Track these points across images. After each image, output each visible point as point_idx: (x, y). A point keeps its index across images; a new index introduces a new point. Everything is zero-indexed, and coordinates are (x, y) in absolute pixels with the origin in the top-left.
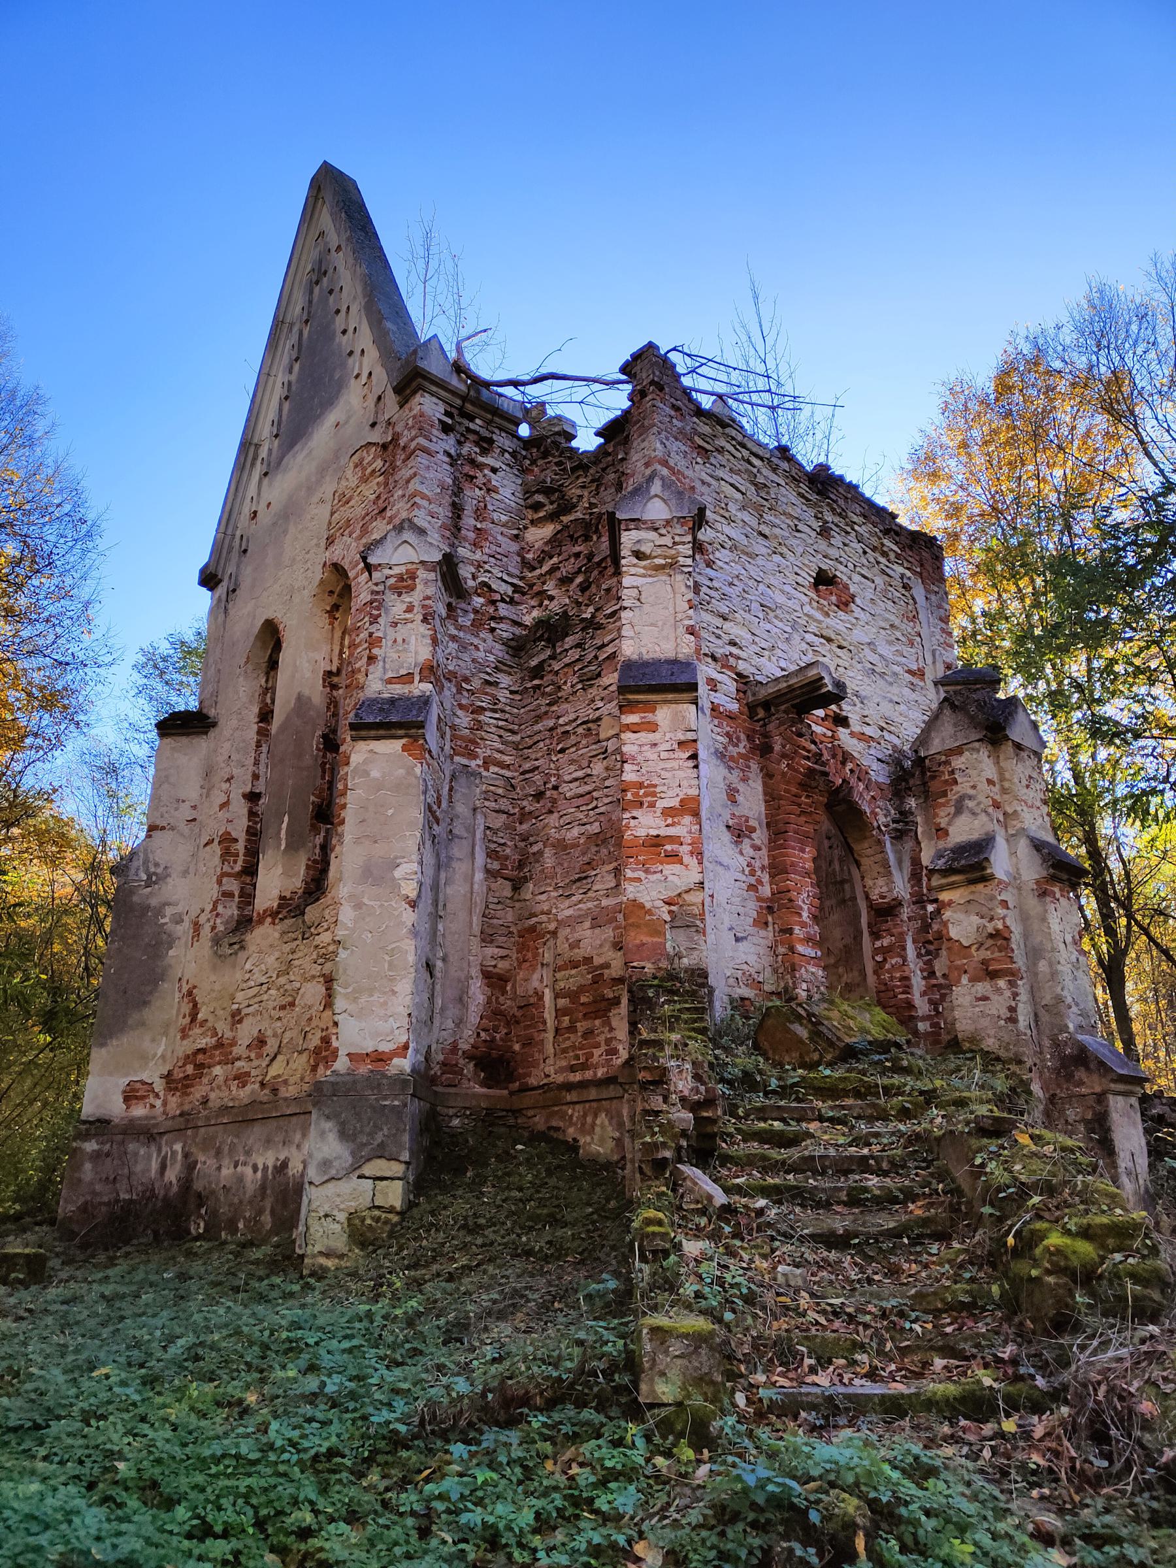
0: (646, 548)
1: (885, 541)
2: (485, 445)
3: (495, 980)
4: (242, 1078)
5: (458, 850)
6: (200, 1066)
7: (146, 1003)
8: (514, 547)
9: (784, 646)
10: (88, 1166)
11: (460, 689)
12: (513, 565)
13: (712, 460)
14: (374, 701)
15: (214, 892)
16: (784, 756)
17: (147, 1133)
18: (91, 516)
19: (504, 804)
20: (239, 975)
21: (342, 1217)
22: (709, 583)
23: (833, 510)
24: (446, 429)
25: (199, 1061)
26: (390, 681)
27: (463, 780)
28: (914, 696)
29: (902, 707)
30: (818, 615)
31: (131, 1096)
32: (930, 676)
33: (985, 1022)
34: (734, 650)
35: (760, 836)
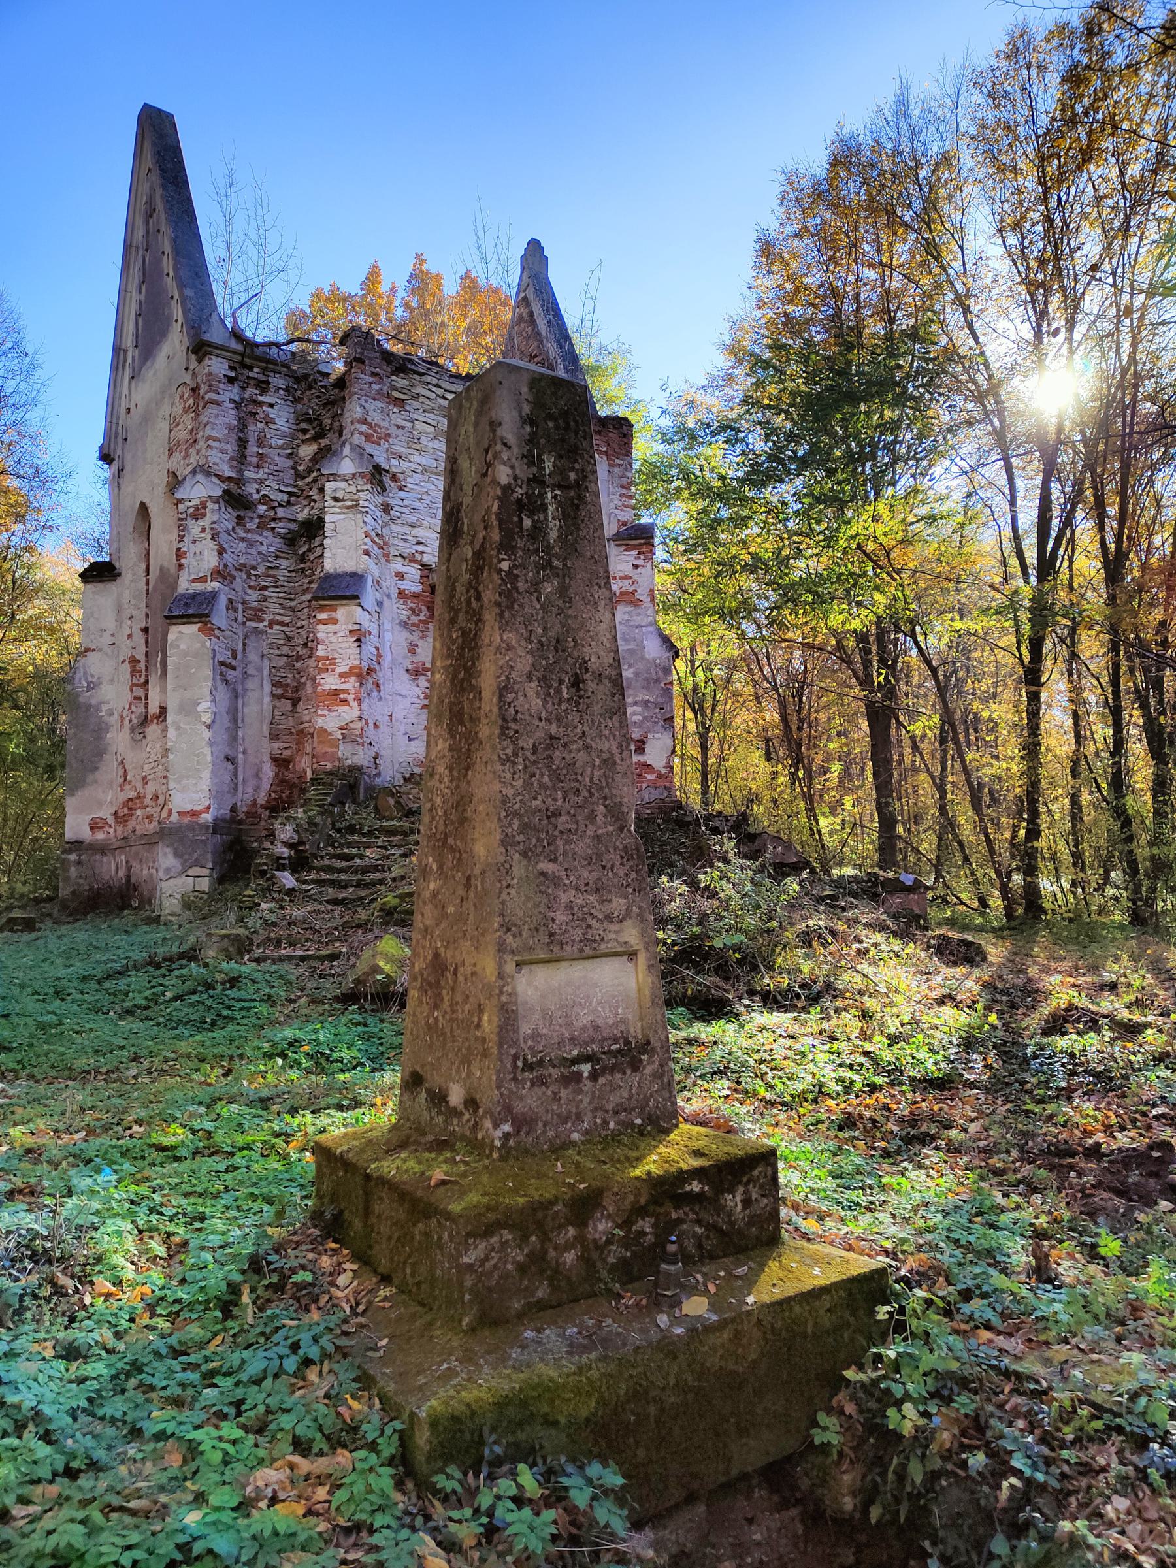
0: (340, 495)
2: (263, 386)
3: (281, 763)
4: (149, 817)
5: (251, 684)
6: (130, 809)
7: (96, 769)
8: (289, 463)
10: (73, 869)
11: (249, 575)
12: (288, 477)
14: (183, 595)
15: (128, 697)
17: (103, 849)
18: (30, 350)
19: (285, 650)
20: (144, 755)
21: (178, 896)
24: (231, 380)
25: (131, 805)
26: (193, 581)
27: (253, 638)
31: (93, 827)
34: (420, 548)
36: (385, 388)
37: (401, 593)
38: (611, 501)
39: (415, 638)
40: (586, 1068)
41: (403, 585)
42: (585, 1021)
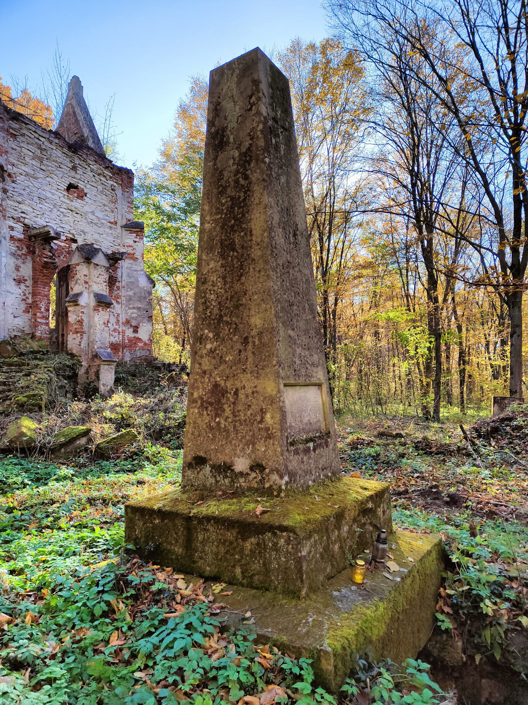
1: (105, 172)
9: (49, 214)
13: (18, 139)
16: (39, 256)
22: (13, 189)
23: (80, 159)
28: (111, 231)
29: (104, 236)
30: (68, 201)
32: (119, 224)
33: (74, 345)
34: (23, 215)
35: (29, 283)
36: (6, 127)
37: (12, 238)
38: (123, 208)
39: (19, 262)
40: (311, 445)
41: (13, 233)
42: (306, 420)
